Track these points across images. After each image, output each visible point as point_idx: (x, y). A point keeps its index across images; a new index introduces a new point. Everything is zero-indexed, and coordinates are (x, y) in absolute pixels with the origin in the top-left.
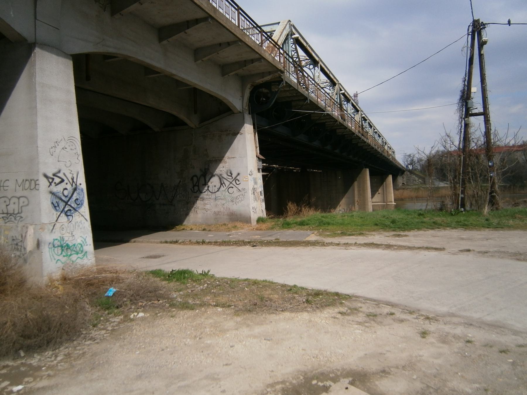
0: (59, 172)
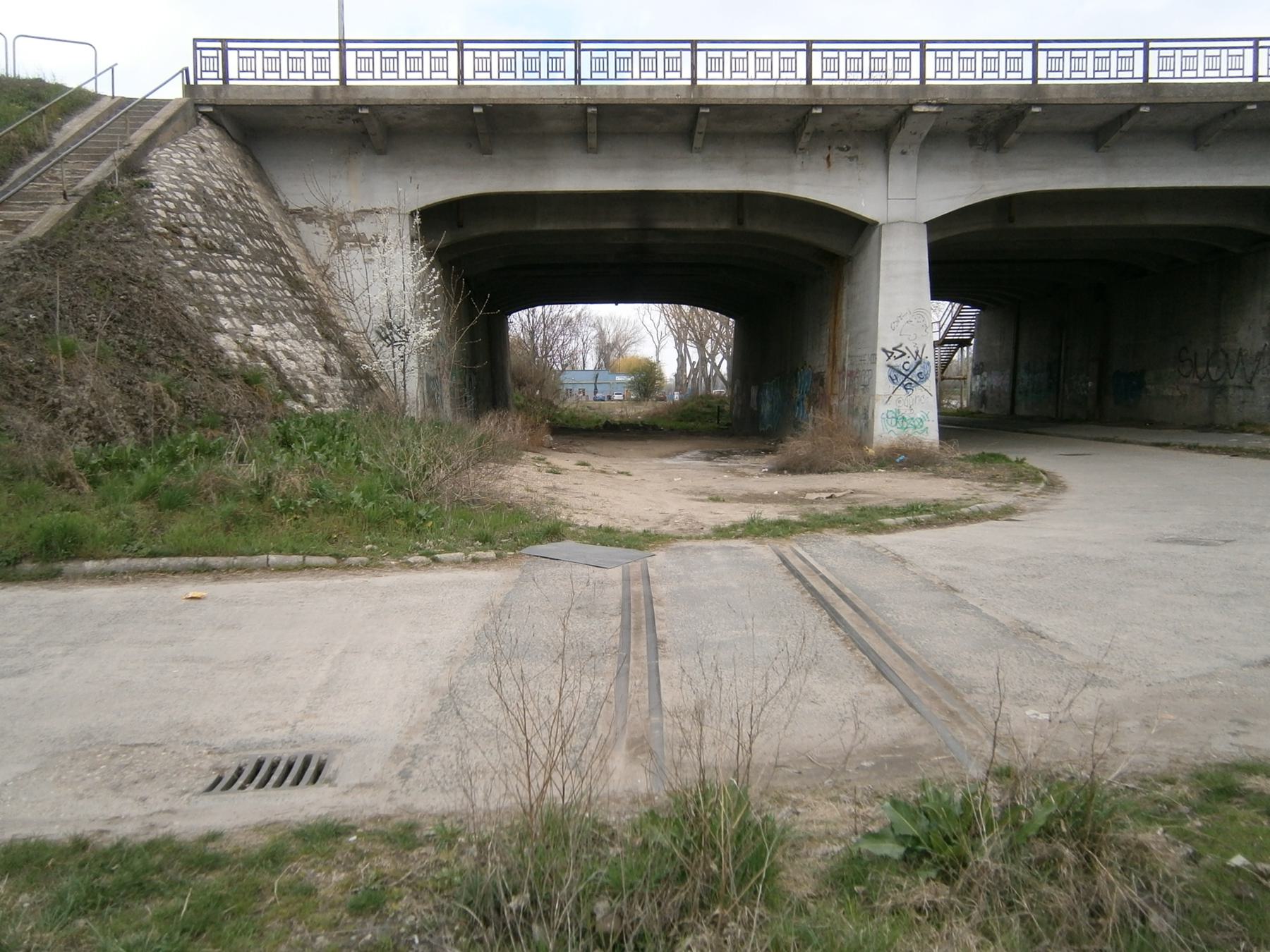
0: (901, 345)
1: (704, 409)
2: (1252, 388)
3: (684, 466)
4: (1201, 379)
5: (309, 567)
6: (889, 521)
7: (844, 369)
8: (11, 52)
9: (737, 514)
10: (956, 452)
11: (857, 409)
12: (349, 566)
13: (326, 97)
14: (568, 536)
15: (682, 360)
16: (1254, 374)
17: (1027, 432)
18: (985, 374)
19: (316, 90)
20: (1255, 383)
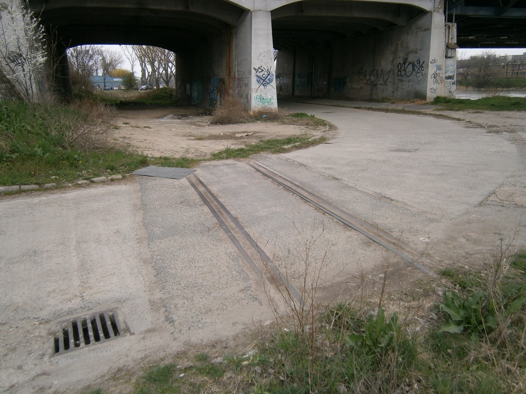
0: (261, 67)
1: (164, 94)
2: (386, 85)
3: (170, 123)
4: (368, 81)
5: (24, 191)
6: (286, 147)
7: (235, 76)
9: (220, 146)
10: (286, 112)
11: (242, 95)
12: (47, 189)
14: (150, 163)
15: (143, 71)
16: (387, 79)
17: (303, 103)
18: (281, 78)
20: (387, 83)
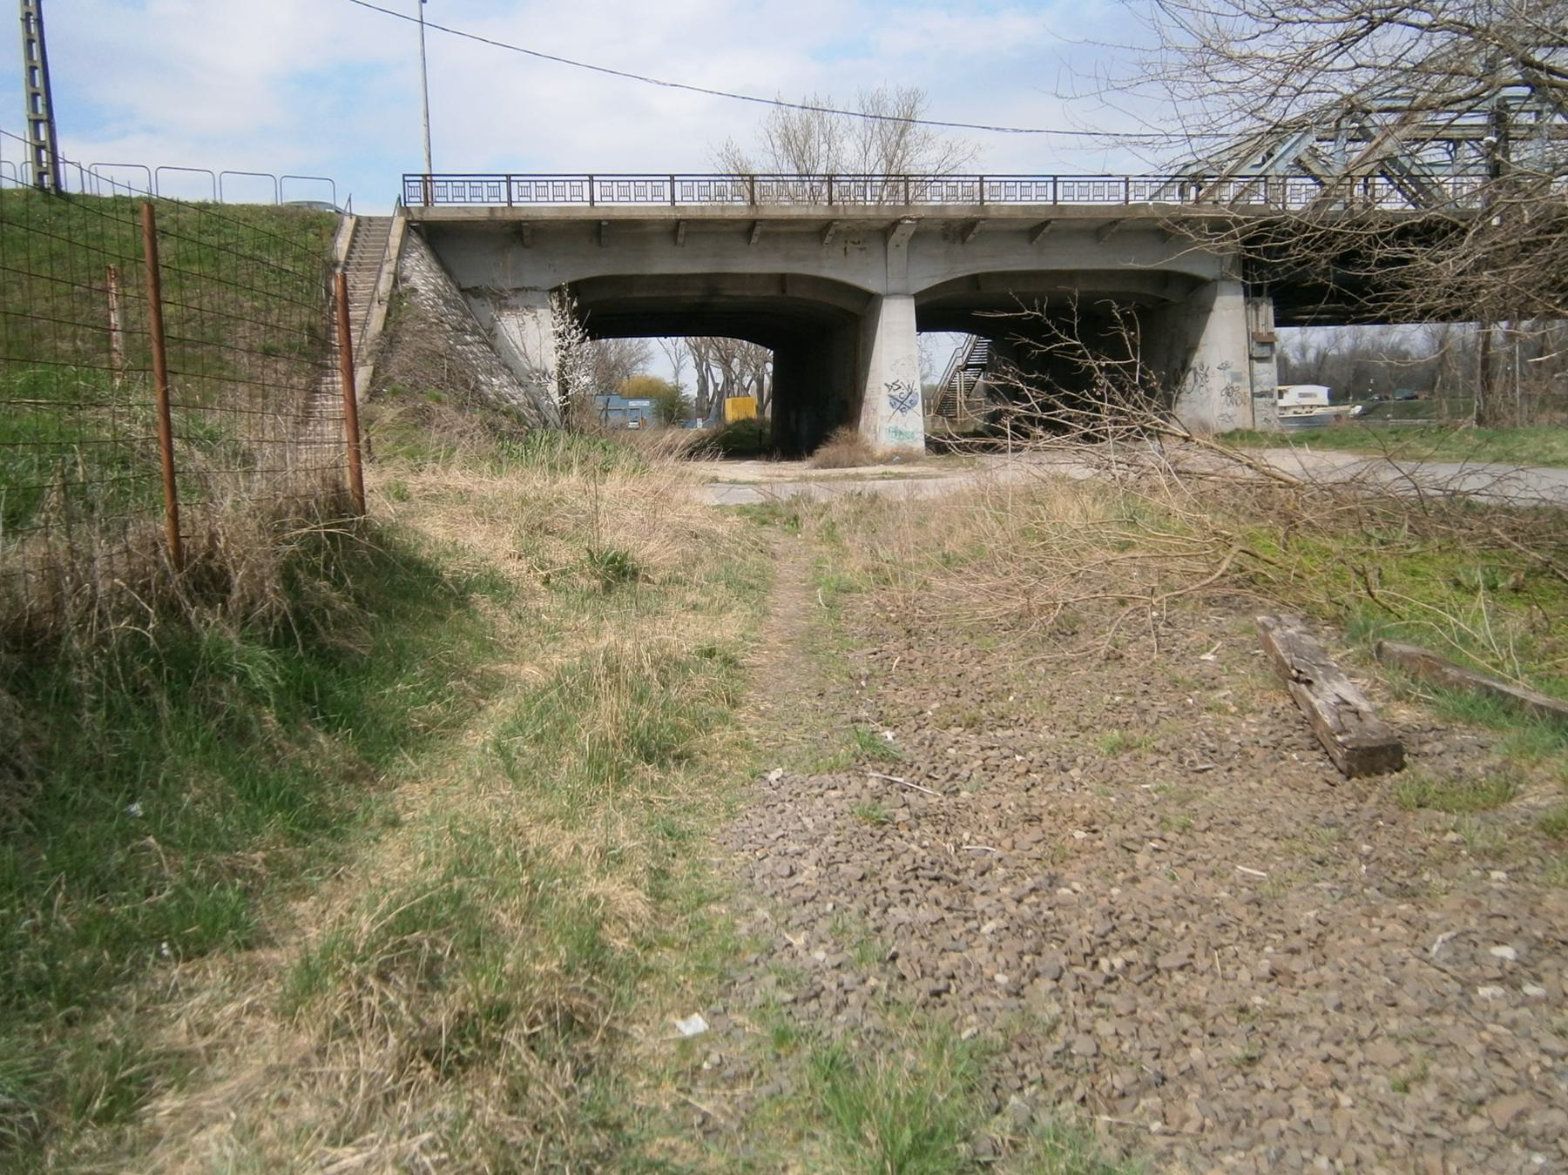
8: (217, 184)
13: (499, 215)
19: (492, 209)
